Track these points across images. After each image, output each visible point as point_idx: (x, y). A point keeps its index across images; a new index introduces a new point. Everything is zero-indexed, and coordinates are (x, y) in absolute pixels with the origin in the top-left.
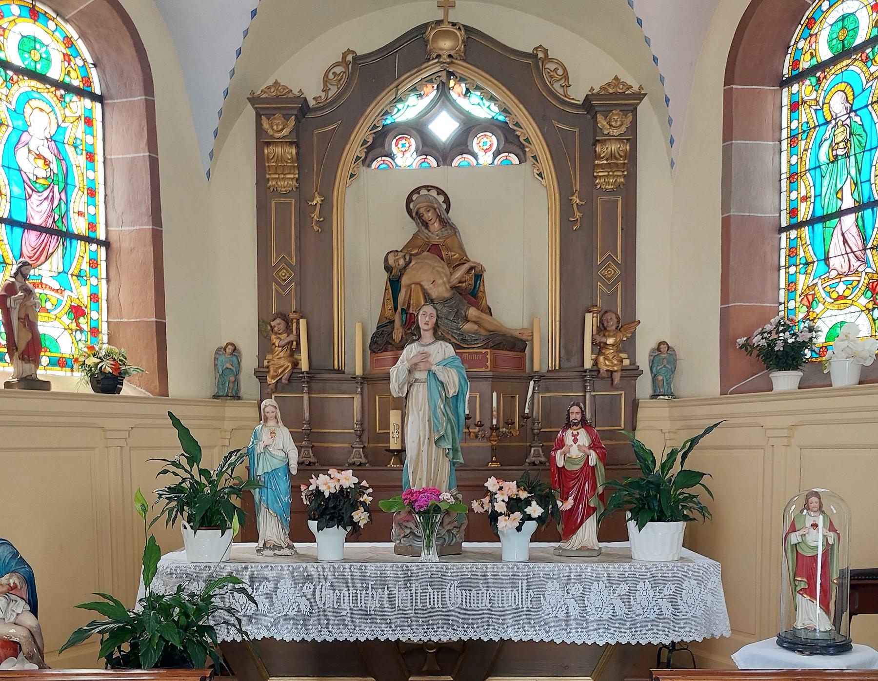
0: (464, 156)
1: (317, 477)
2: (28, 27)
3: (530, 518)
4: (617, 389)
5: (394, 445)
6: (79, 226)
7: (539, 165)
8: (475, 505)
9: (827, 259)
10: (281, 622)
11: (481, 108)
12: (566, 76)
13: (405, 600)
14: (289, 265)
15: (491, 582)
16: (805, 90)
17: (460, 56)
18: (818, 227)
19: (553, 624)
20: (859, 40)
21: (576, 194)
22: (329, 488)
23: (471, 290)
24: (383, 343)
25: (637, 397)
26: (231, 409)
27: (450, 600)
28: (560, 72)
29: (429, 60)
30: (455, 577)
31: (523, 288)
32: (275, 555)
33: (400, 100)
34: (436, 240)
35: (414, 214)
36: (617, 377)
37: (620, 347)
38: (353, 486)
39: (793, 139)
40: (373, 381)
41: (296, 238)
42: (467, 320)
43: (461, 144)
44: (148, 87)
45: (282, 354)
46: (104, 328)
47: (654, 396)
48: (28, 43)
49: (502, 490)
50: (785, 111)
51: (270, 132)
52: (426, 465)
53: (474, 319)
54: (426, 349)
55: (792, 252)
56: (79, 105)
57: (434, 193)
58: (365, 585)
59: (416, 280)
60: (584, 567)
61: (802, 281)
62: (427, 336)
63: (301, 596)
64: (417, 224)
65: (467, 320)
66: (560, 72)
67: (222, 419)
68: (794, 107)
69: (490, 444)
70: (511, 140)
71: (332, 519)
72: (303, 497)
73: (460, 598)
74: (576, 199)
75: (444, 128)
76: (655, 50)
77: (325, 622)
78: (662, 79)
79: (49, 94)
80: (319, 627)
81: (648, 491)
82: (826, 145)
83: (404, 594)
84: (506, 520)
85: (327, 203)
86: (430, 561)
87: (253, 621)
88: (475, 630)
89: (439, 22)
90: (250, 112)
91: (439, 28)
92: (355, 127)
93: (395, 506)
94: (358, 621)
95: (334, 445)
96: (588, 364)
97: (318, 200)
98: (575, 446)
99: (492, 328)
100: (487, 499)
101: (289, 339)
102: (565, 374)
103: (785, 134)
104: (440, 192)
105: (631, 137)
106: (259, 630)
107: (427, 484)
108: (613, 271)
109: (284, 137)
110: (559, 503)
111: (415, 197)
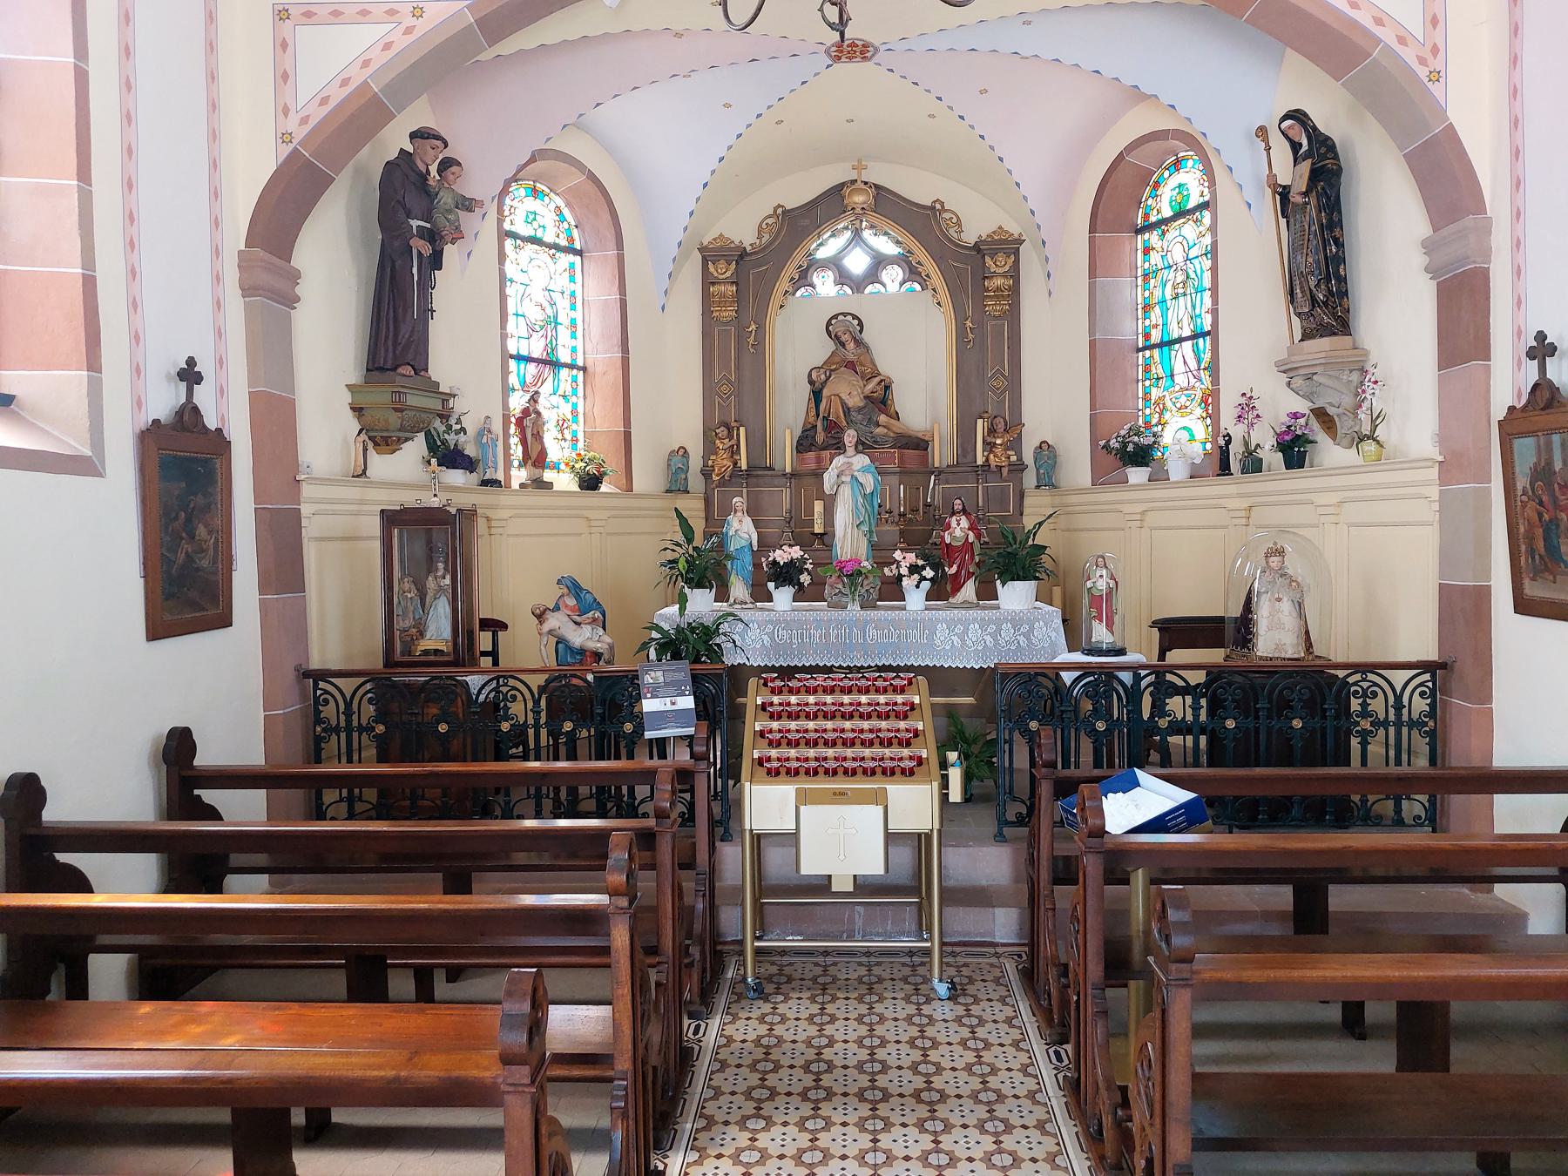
2: (532, 204)
3: (925, 579)
5: (818, 529)
6: (564, 357)
9: (1172, 376)
11: (887, 247)
12: (959, 223)
14: (729, 381)
16: (1153, 238)
18: (1166, 349)
20: (1191, 205)
23: (881, 400)
30: (872, 620)
34: (851, 357)
36: (1005, 471)
37: (1007, 447)
39: (1146, 277)
43: (873, 275)
44: (620, 245)
46: (581, 436)
47: (1038, 487)
48: (532, 217)
49: (905, 559)
50: (1140, 253)
52: (849, 542)
55: (1147, 369)
56: (565, 259)
61: (1155, 393)
62: (850, 451)
68: (1146, 251)
70: (913, 272)
74: (969, 323)
75: (857, 263)
76: (1031, 204)
78: (1039, 227)
79: (543, 255)
81: (1013, 558)
82: (1169, 285)
85: (761, 328)
96: (980, 461)
103: (1140, 273)
104: (855, 317)
105: (1015, 274)
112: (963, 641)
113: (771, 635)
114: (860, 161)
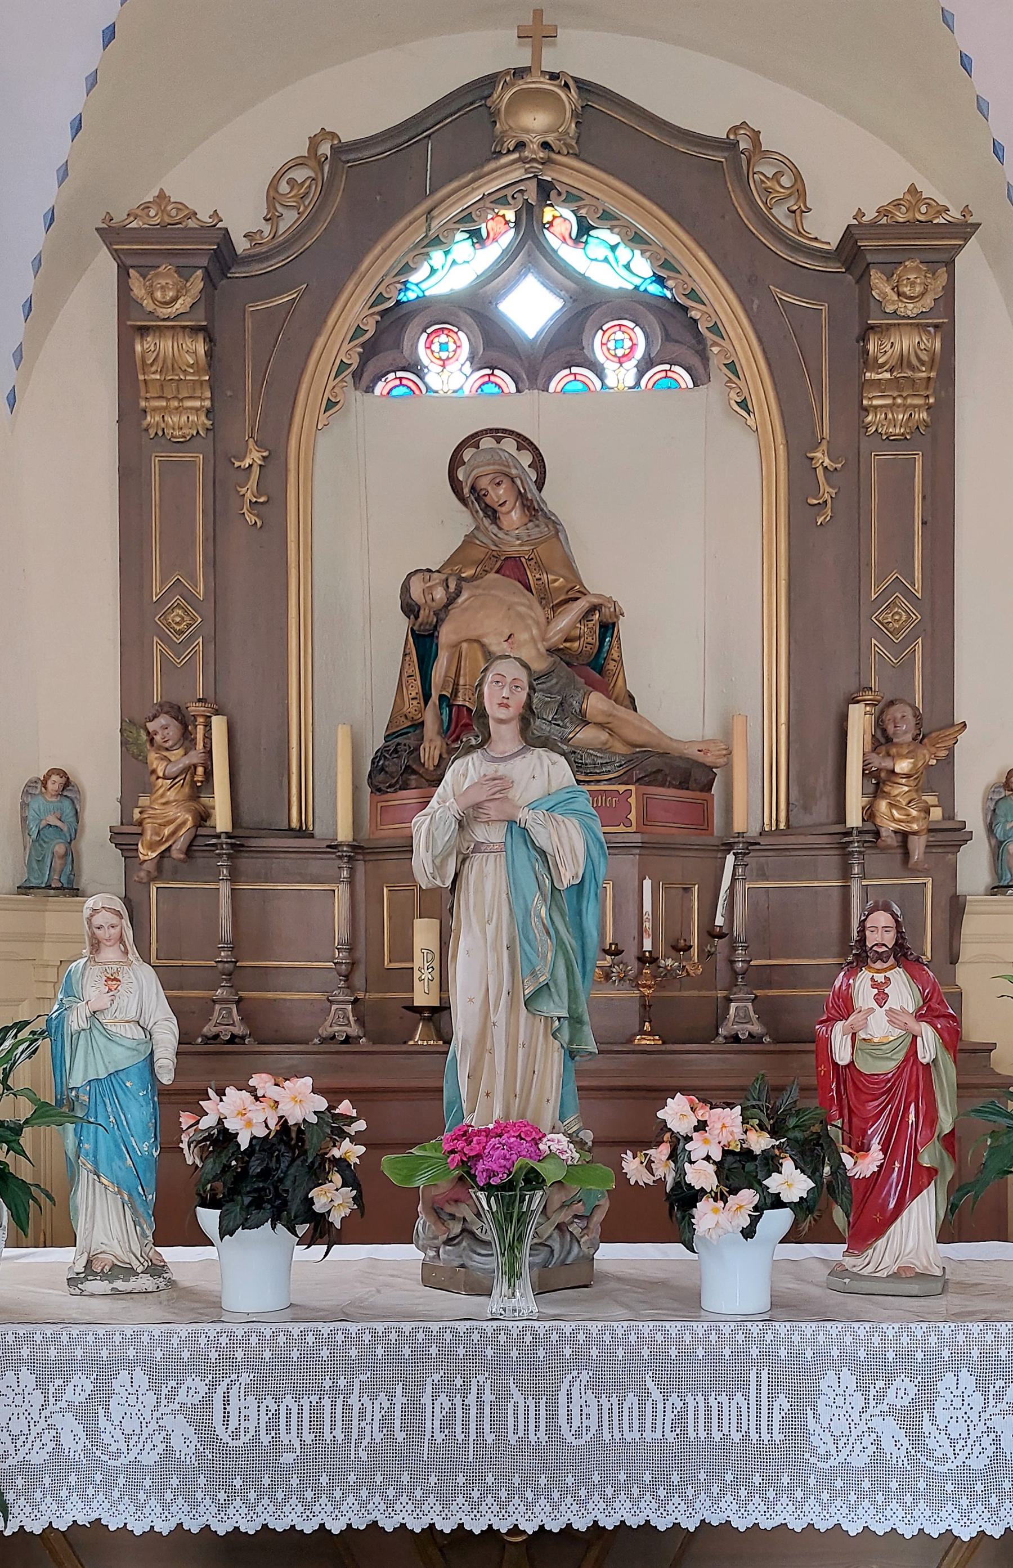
0: (574, 370)
1: (221, 1093)
3: (777, 1203)
4: (915, 872)
5: (423, 996)
7: (742, 384)
8: (632, 1166)
10: (121, 1481)
11: (612, 264)
12: (799, 190)
13: (447, 1423)
14: (190, 598)
15: (674, 1373)
17: (568, 146)
19: (839, 1483)
21: (824, 446)
22: (249, 1123)
23: (591, 656)
24: (399, 769)
25: (961, 889)
26: (57, 917)
27: (569, 1421)
28: (786, 181)
29: (499, 154)
31: (705, 648)
32: (116, 1293)
33: (436, 242)
34: (513, 547)
35: (466, 491)
36: (918, 846)
38: (314, 1119)
40: (373, 855)
41: (205, 540)
42: (583, 720)
43: (567, 345)
45: (171, 795)
47: (997, 889)
51: (148, 304)
52: (507, 1064)
53: (600, 719)
54: (502, 769)
57: (509, 445)
58: (342, 1382)
59: (473, 634)
60: (919, 1333)
62: (505, 736)
63: (174, 1413)
64: (474, 513)
65: (583, 720)
66: (786, 181)
67: (38, 938)
69: (636, 993)
70: (677, 331)
71: (257, 1204)
72: (184, 1146)
73: (594, 1417)
75: (531, 309)
77: (238, 1482)
80: (222, 1496)
83: (447, 1405)
84: (716, 1211)
85: (275, 462)
86: (516, 1316)
87: (47, 1481)
88: (635, 1502)
89: (519, 73)
90: (104, 266)
91: (521, 85)
92: (336, 299)
93: (423, 1170)
94: (324, 1479)
95: (288, 996)
96: (854, 819)
97: (254, 456)
98: (880, 1013)
99: (640, 739)
100: (665, 1150)
101: (186, 761)
102: (801, 839)
104: (524, 443)
105: (941, 321)
106: (60, 1502)
107: (507, 1115)
108: (903, 615)
109: (178, 317)
110: (847, 1160)
111: (467, 454)
112: (917, 1437)
113: (199, 1415)
114: (538, 14)
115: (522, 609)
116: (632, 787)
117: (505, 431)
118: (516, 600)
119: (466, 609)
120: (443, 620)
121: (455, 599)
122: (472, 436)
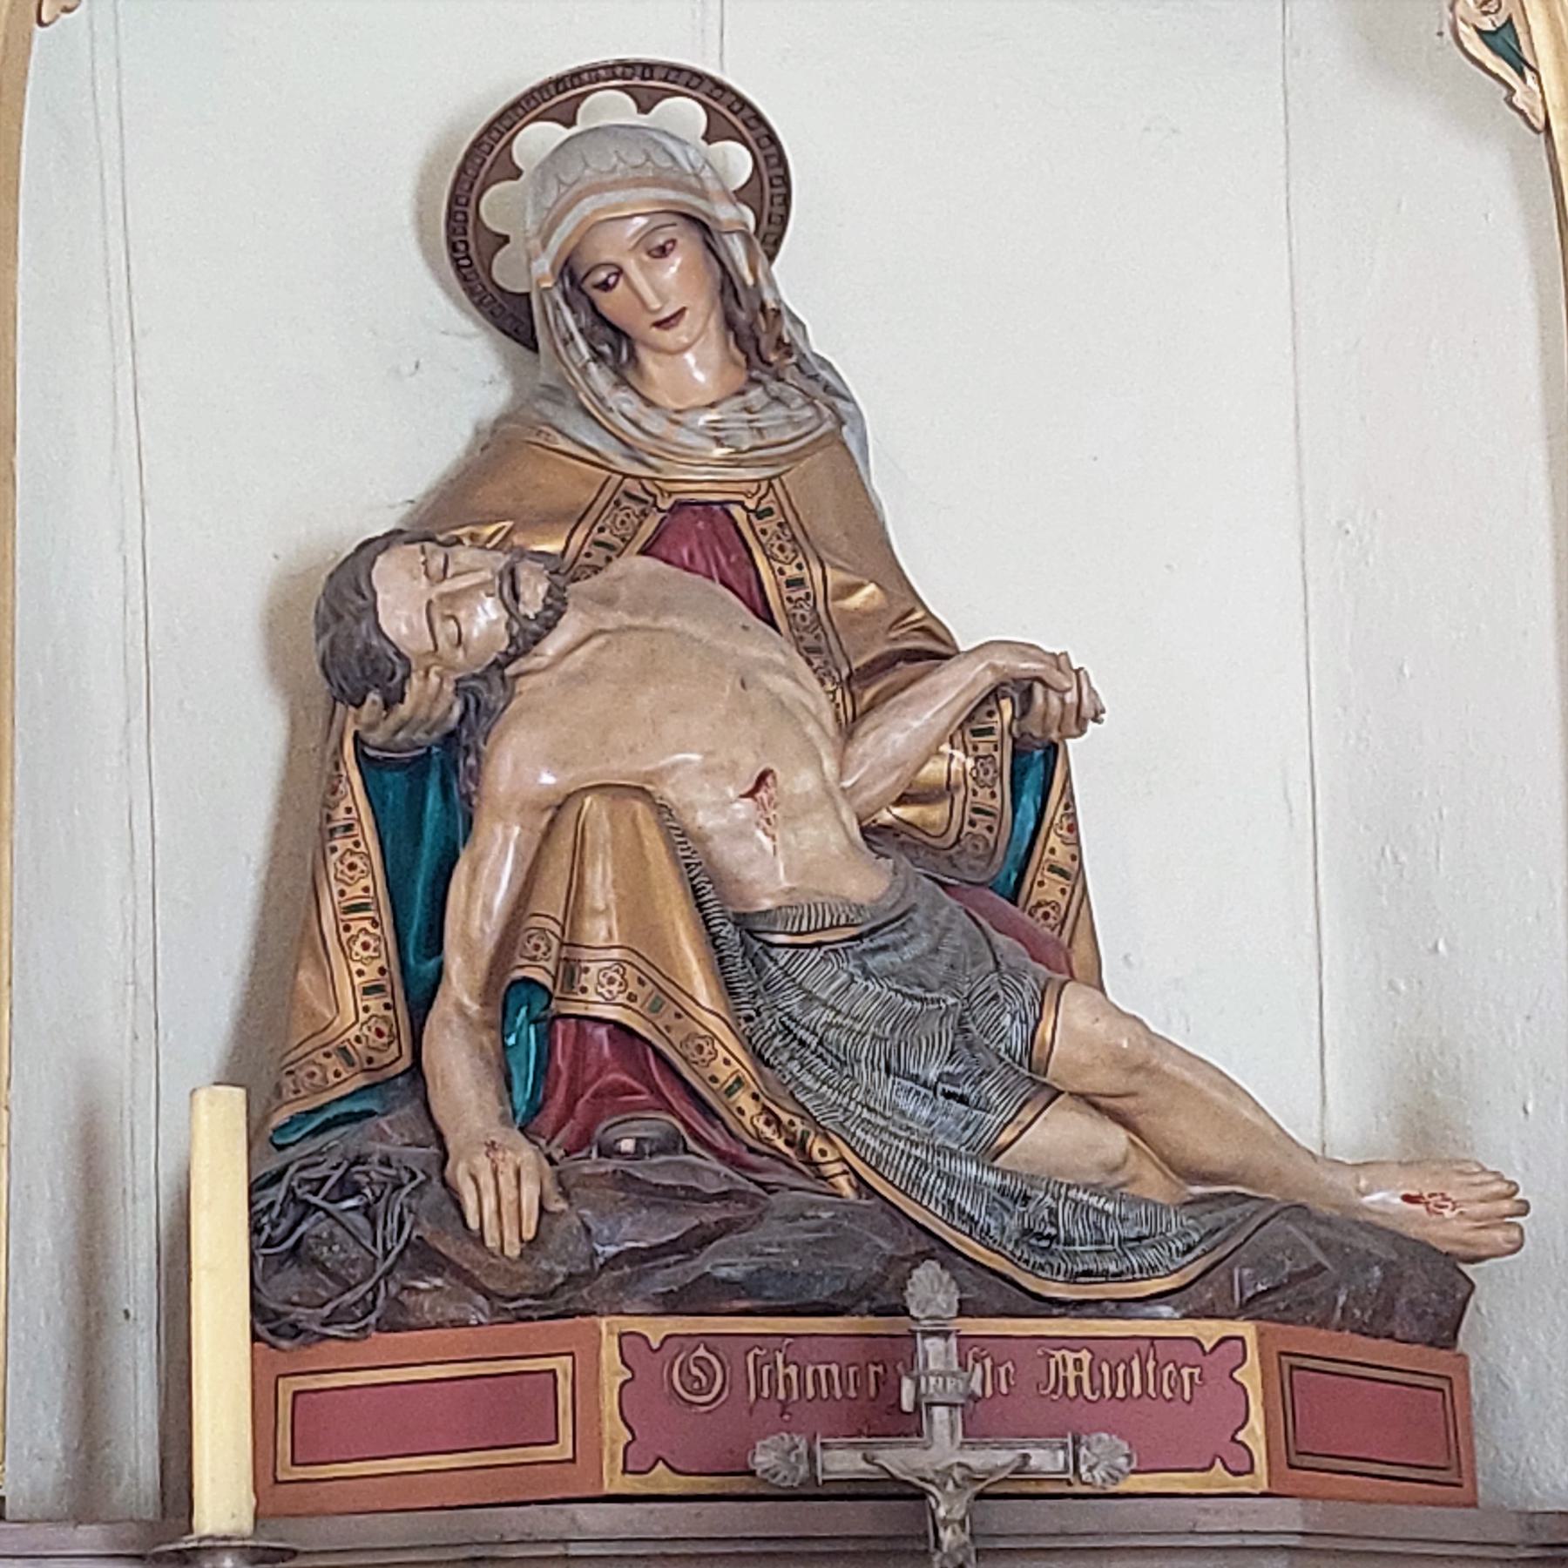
34: (701, 468)
53: (1100, 1080)
57: (684, 114)
59: (620, 769)
111: (537, 140)
115: (781, 684)
116: (1245, 1329)
117: (575, 77)
118: (755, 652)
119: (583, 677)
120: (493, 714)
121: (537, 639)
122: (559, 83)
